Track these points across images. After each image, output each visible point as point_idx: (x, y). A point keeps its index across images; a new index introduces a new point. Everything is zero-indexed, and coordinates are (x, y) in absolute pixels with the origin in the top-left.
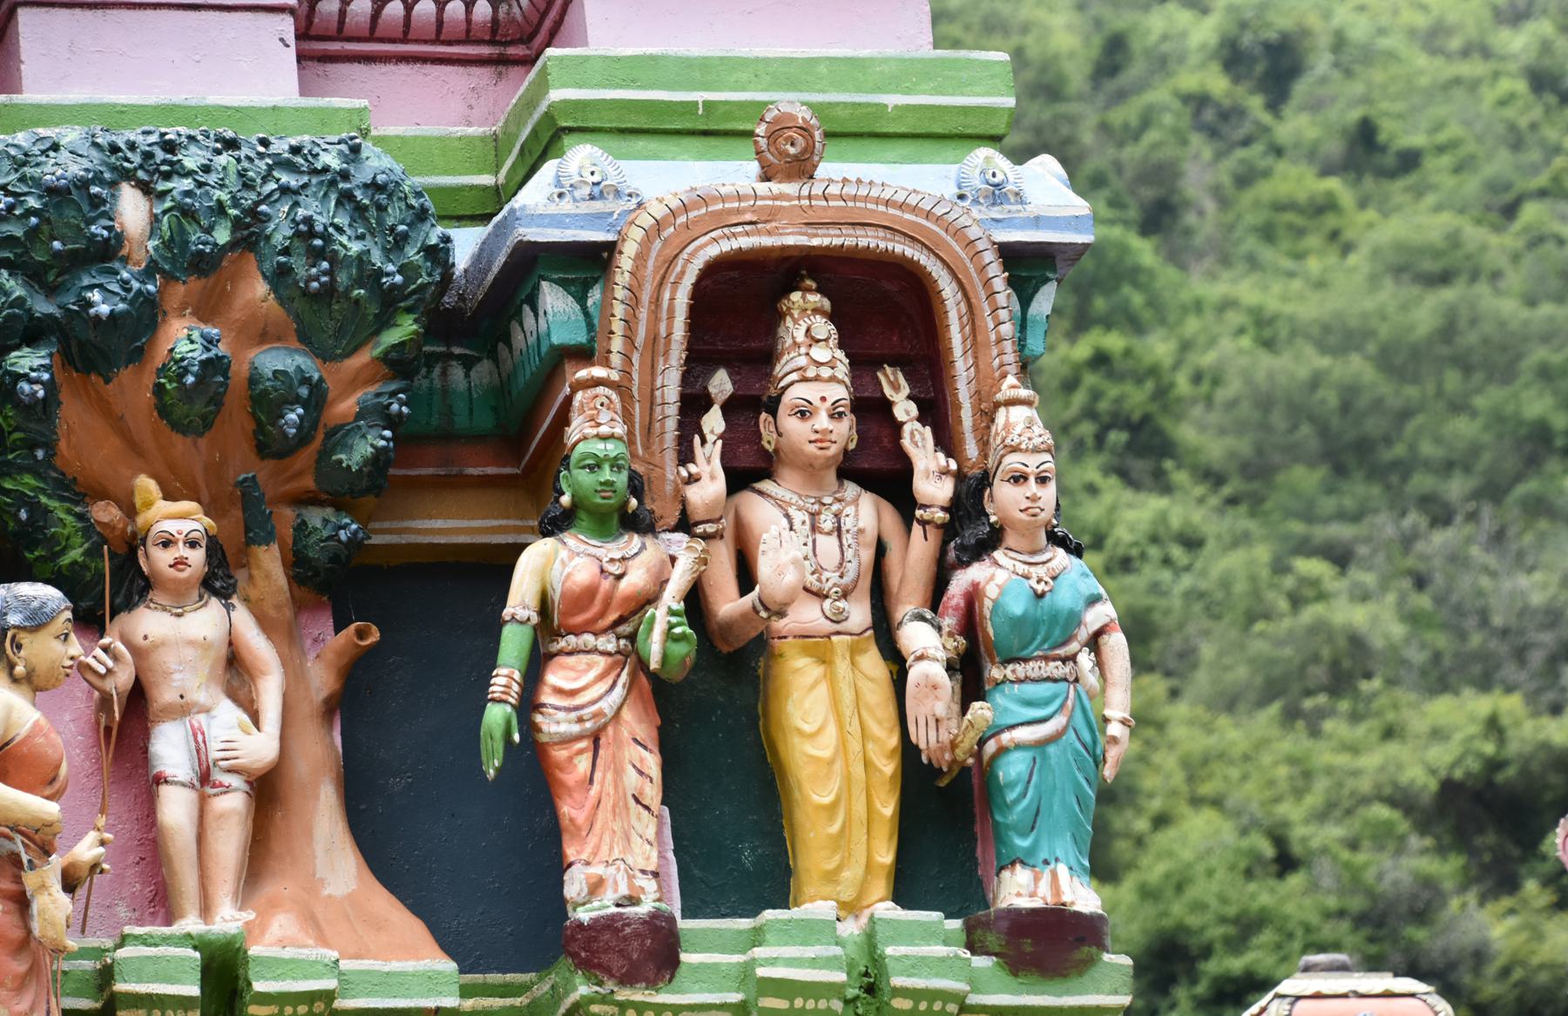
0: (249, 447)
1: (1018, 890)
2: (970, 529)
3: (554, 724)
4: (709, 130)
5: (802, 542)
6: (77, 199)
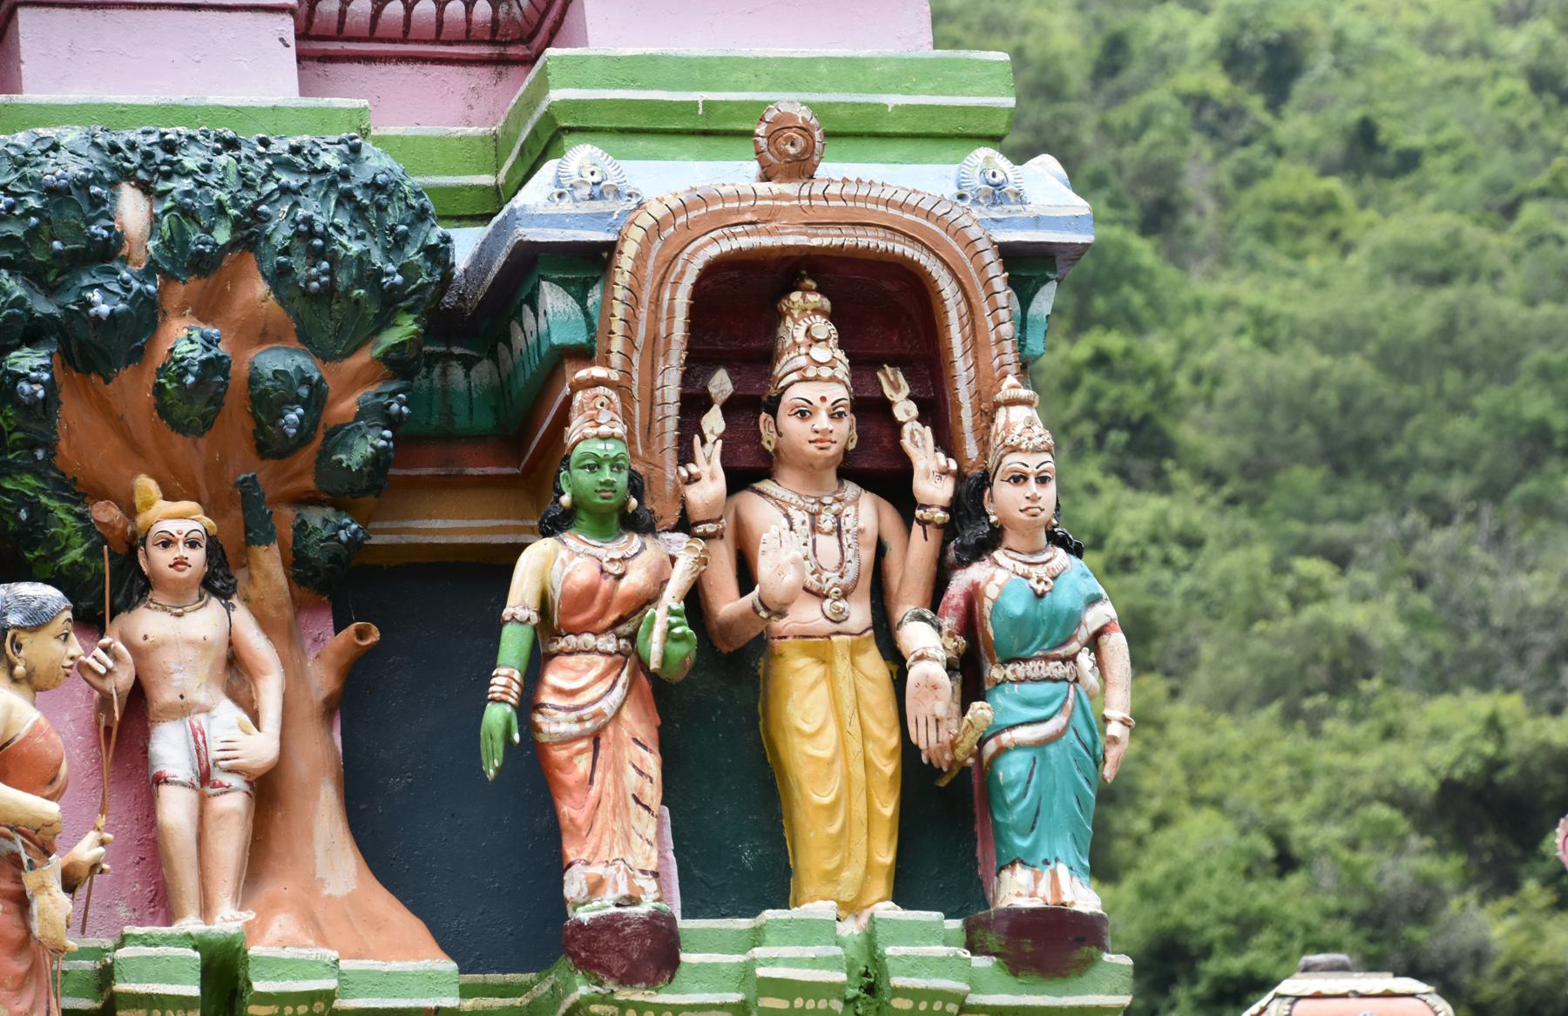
0: (249, 447)
1: (1018, 890)
2: (970, 529)
3: (554, 724)
4: (709, 130)
5: (802, 542)
6: (77, 199)
